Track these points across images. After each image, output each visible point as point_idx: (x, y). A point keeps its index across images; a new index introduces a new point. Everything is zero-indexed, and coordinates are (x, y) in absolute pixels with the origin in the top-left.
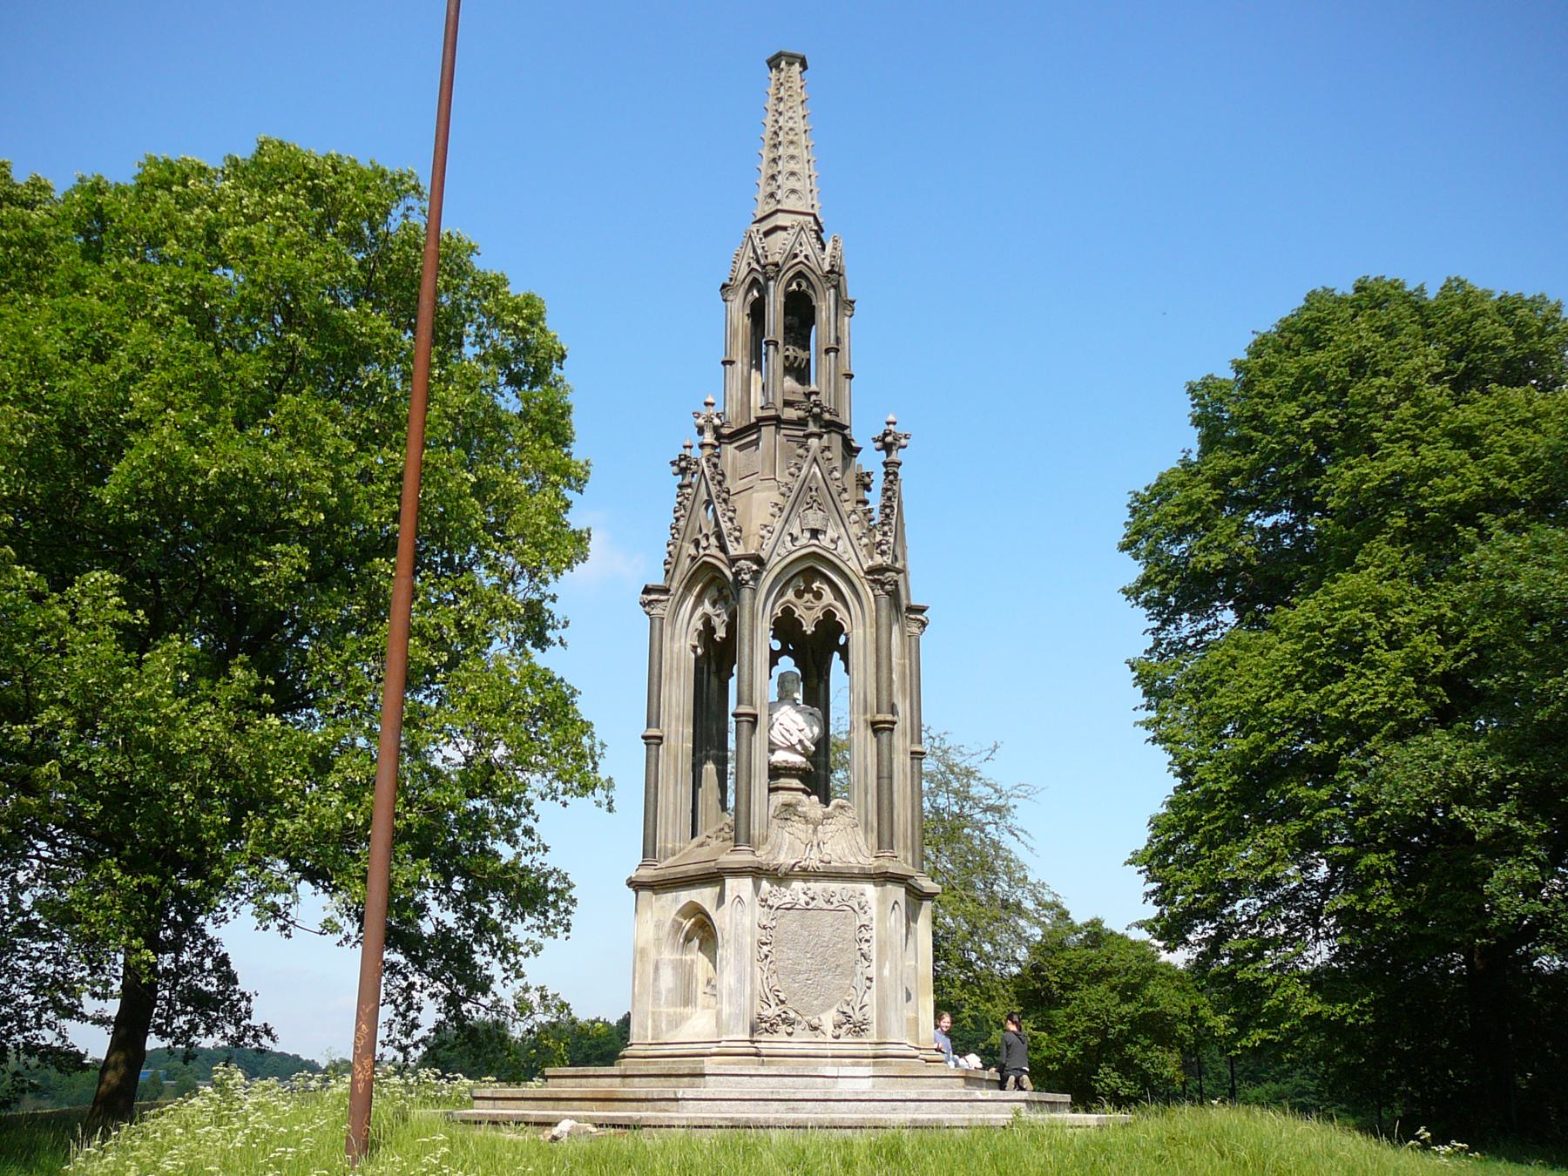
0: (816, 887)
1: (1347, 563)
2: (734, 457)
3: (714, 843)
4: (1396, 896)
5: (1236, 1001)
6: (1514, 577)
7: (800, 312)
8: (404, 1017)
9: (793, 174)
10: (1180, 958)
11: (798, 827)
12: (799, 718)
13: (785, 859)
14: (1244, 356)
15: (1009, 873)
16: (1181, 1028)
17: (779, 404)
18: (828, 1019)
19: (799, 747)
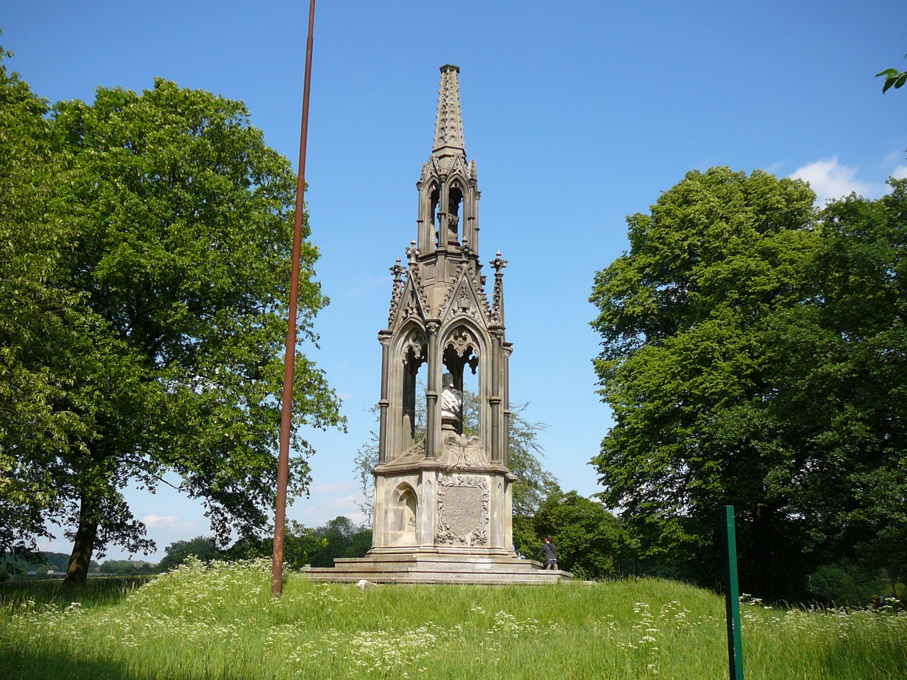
0: (464, 476)
1: (705, 315)
3: (414, 455)
4: (721, 482)
5: (642, 531)
6: (785, 330)
7: (456, 196)
8: (221, 536)
9: (453, 128)
10: (617, 512)
11: (456, 448)
12: (453, 396)
13: (450, 463)
14: (655, 204)
15: (531, 466)
16: (615, 545)
17: (446, 243)
18: (468, 537)
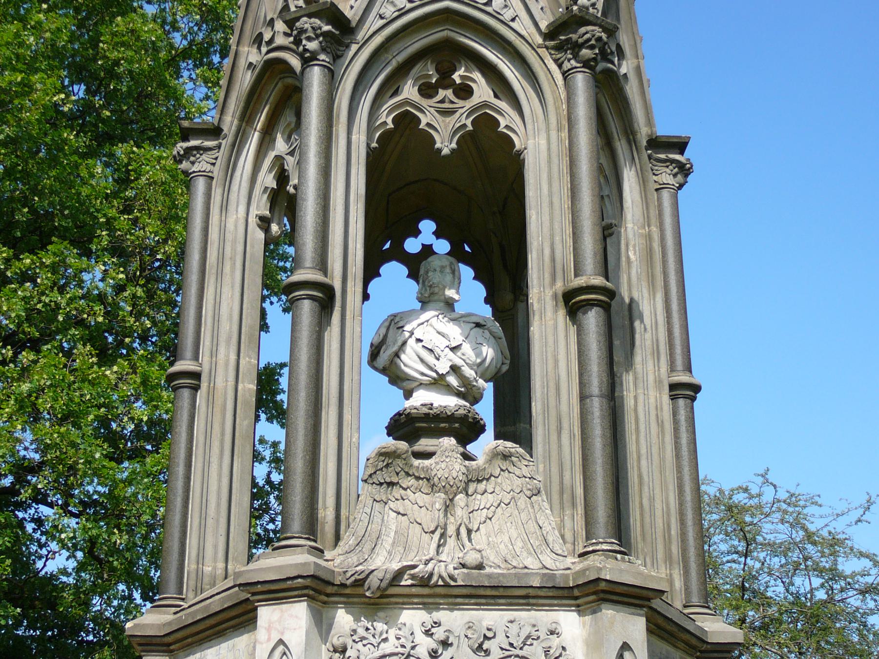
0: (454, 620)
13: (383, 562)
19: (452, 380)
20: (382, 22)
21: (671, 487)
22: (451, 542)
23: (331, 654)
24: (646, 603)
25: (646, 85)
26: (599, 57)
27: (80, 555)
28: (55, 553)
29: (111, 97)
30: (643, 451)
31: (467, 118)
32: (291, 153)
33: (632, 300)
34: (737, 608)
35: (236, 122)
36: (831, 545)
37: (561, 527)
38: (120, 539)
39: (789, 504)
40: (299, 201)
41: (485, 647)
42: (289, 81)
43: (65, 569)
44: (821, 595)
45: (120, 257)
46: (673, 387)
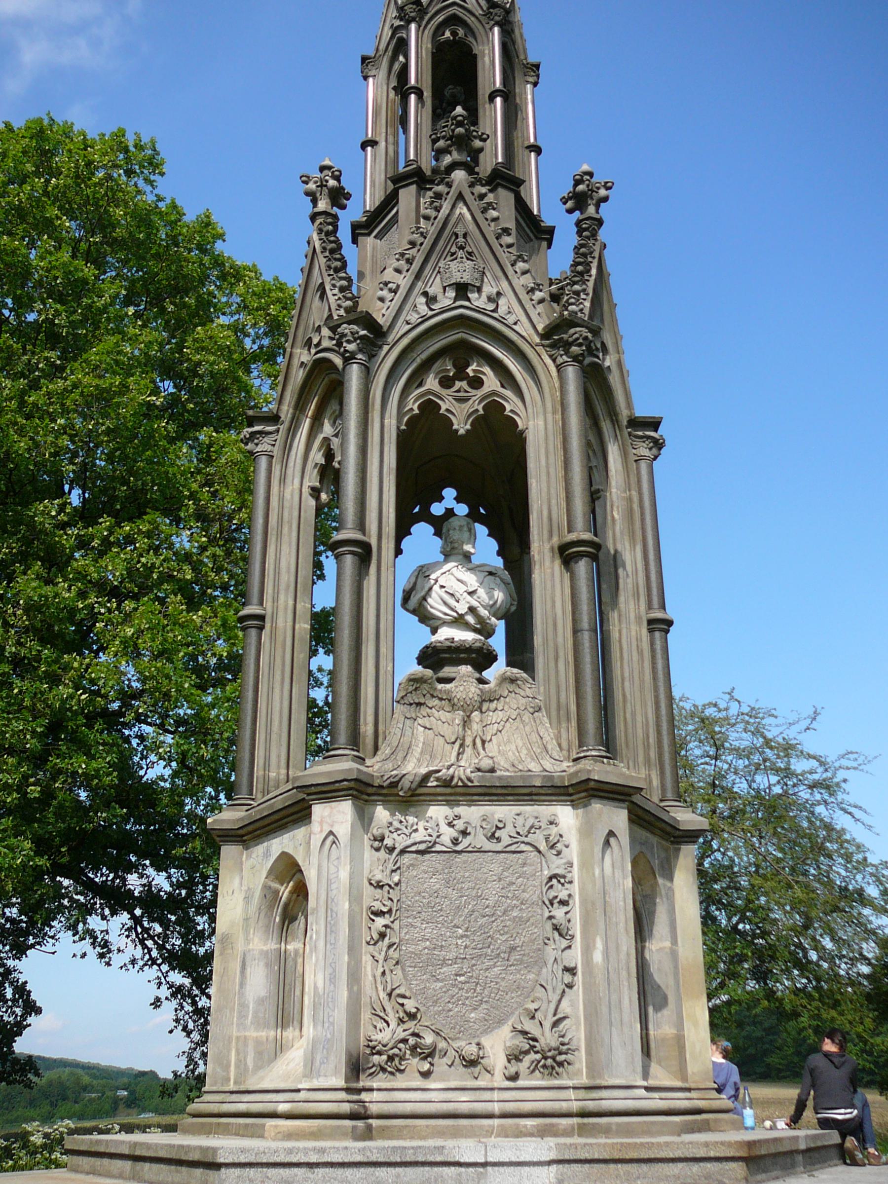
0: (471, 814)
2: (374, 248)
13: (413, 767)
15: (848, 858)
18: (496, 1046)
19: (470, 619)
20: (410, 326)
21: (649, 704)
22: (469, 751)
23: (371, 842)
24: (628, 798)
25: (625, 375)
26: (586, 353)
27: (174, 764)
28: (154, 763)
29: (194, 393)
30: (627, 675)
31: (479, 403)
32: (336, 435)
33: (616, 551)
34: (709, 801)
35: (291, 411)
36: (786, 749)
37: (558, 737)
38: (206, 752)
39: (751, 717)
40: (342, 474)
41: (497, 835)
42: (334, 376)
43: (162, 776)
44: (777, 790)
45: (203, 521)
46: (650, 622)
